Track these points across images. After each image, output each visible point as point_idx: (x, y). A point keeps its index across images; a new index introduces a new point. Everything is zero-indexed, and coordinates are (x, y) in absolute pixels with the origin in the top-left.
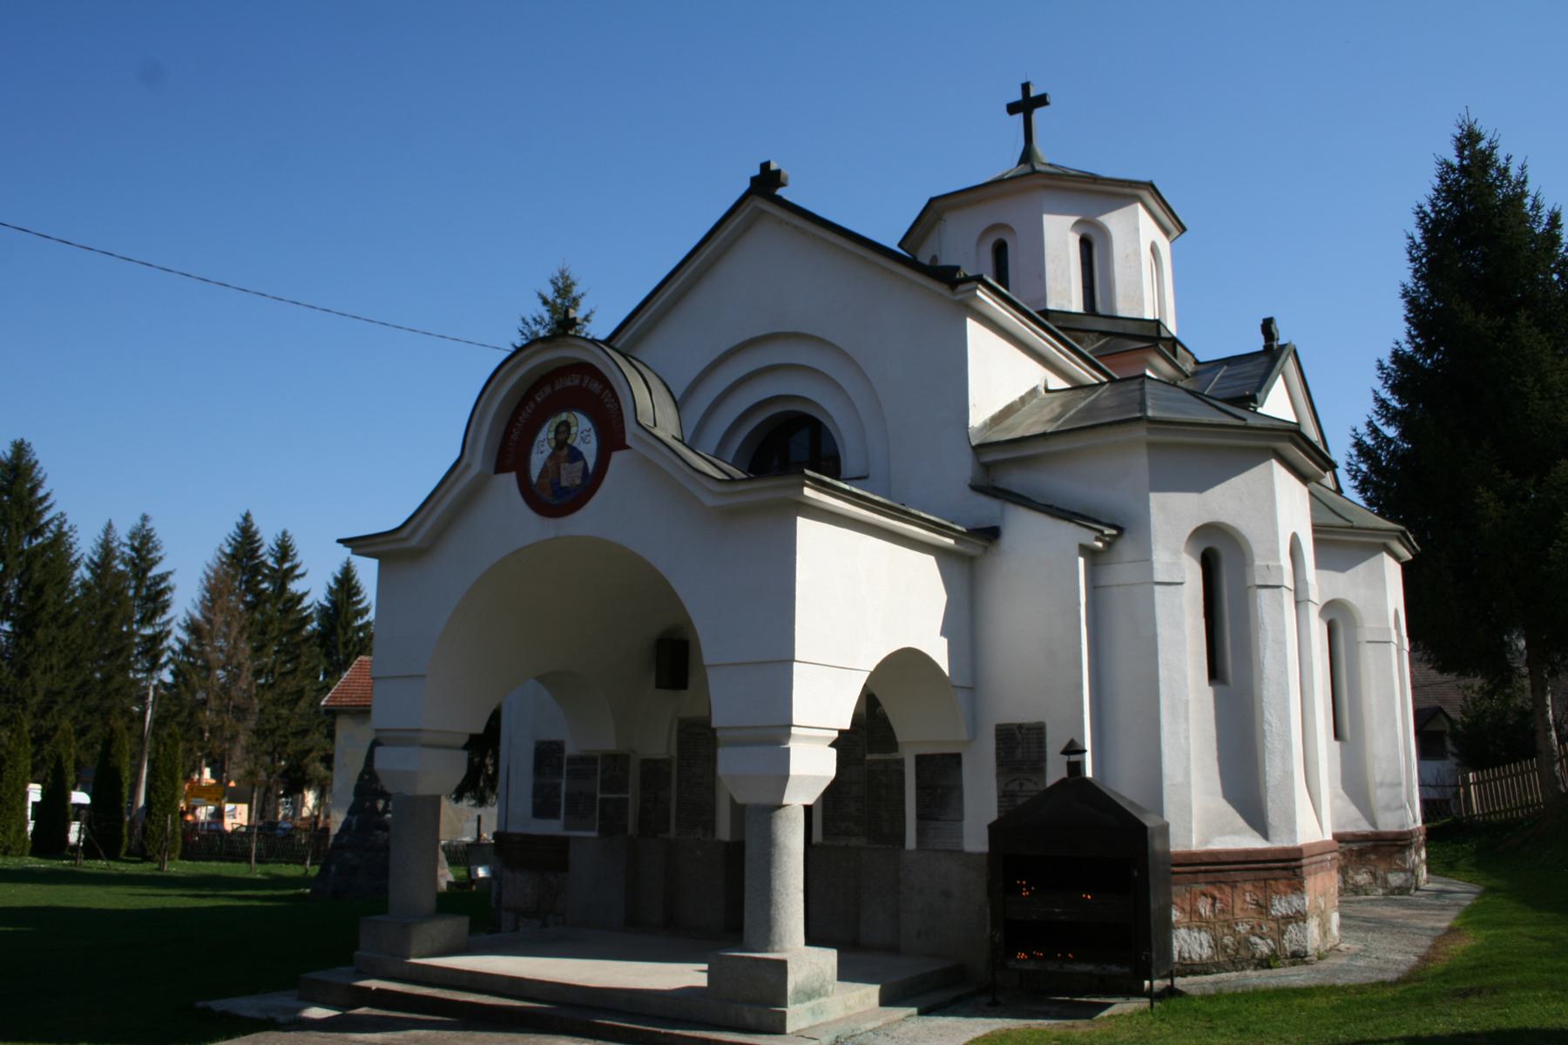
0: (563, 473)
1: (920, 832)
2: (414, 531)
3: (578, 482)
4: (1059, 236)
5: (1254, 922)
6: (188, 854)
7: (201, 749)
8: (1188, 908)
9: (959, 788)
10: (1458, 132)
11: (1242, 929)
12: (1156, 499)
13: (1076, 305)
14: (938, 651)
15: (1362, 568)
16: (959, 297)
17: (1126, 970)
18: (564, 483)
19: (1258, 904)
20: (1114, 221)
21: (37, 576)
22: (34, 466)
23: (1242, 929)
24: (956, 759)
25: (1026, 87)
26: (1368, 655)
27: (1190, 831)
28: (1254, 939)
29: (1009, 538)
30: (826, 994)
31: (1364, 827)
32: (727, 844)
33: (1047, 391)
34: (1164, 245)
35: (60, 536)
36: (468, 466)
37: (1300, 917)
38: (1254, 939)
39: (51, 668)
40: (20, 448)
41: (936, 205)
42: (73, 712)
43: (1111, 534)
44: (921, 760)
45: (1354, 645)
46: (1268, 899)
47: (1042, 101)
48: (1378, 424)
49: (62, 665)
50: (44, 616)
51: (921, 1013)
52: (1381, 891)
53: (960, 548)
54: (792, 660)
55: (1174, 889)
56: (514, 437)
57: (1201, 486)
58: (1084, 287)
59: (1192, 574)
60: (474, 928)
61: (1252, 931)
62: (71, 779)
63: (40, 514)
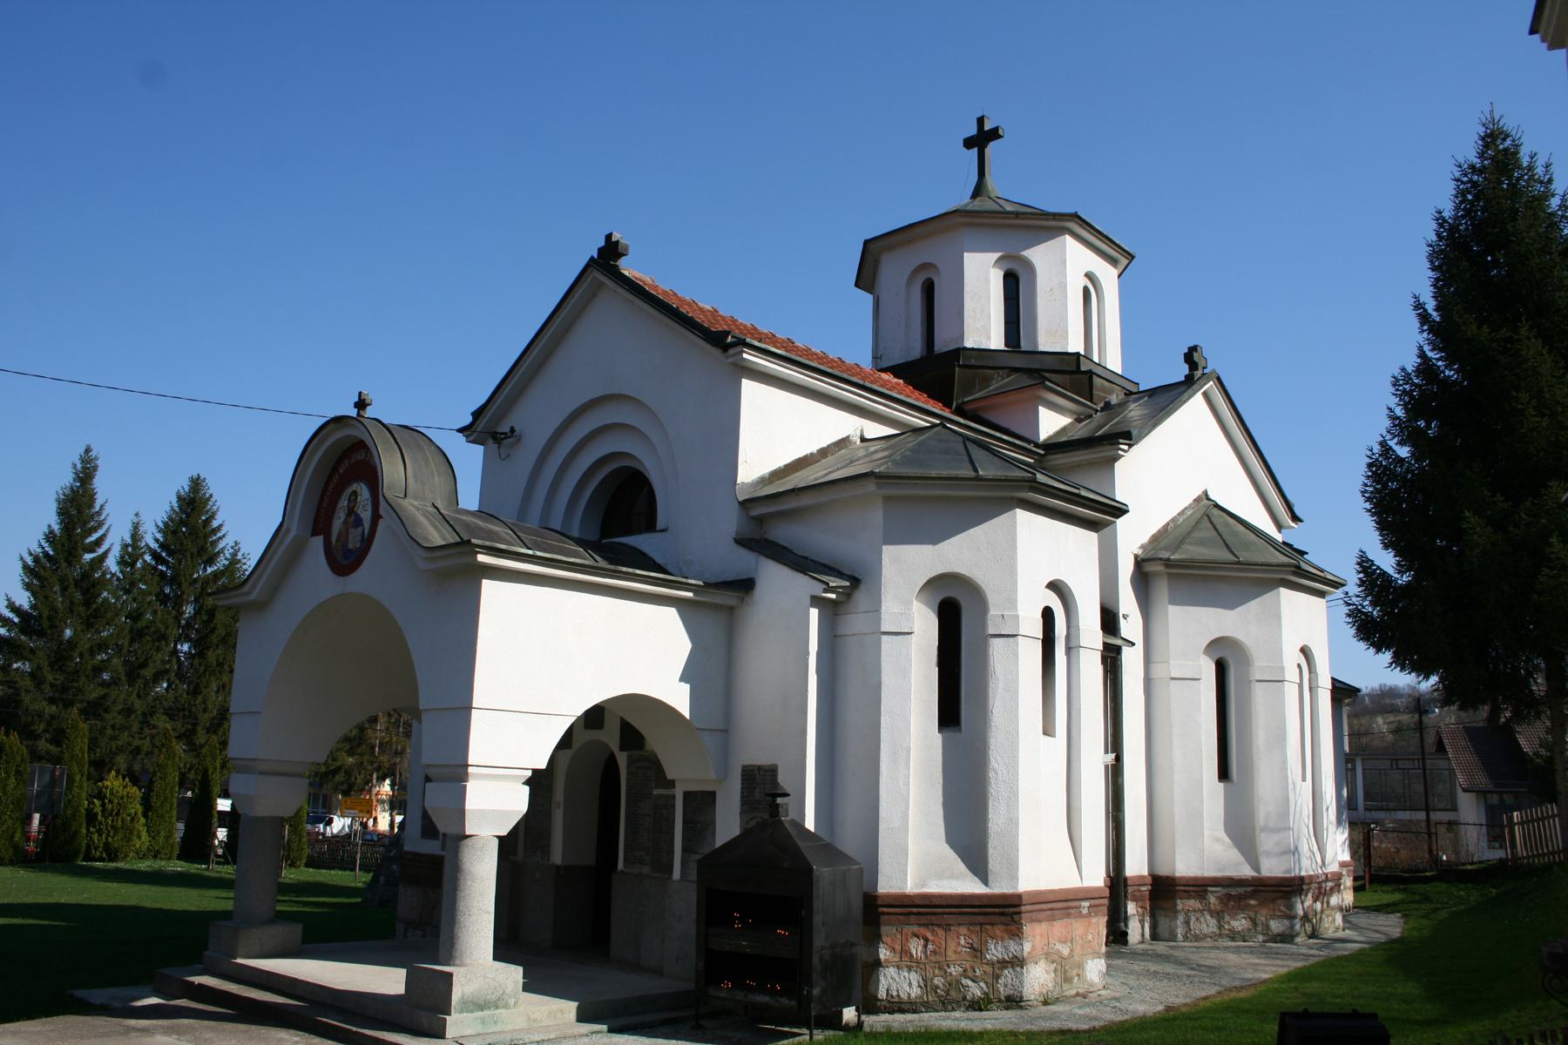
2: (254, 587)
4: (981, 276)
5: (968, 966)
6: (312, 863)
7: (372, 763)
8: (898, 948)
9: (714, 823)
10: (1482, 130)
11: (954, 970)
12: (888, 552)
13: (996, 341)
14: (679, 698)
15: (1254, 606)
17: (793, 1003)
18: (350, 546)
19: (972, 947)
20: (1039, 255)
23: (954, 970)
25: (981, 121)
26: (1260, 694)
27: (906, 874)
28: (964, 981)
30: (506, 1006)
31: (1247, 872)
32: (558, 867)
33: (863, 440)
34: (1108, 275)
35: (234, 561)
36: (288, 531)
37: (1018, 962)
38: (964, 981)
41: (871, 246)
43: (846, 587)
44: (687, 795)
45: (1246, 683)
46: (984, 943)
47: (995, 134)
48: (1392, 443)
50: (214, 639)
51: (611, 1031)
52: (1261, 938)
54: (471, 708)
55: (884, 929)
57: (935, 538)
58: (1006, 323)
59: (925, 626)
61: (965, 974)
62: (217, 790)
63: (214, 543)
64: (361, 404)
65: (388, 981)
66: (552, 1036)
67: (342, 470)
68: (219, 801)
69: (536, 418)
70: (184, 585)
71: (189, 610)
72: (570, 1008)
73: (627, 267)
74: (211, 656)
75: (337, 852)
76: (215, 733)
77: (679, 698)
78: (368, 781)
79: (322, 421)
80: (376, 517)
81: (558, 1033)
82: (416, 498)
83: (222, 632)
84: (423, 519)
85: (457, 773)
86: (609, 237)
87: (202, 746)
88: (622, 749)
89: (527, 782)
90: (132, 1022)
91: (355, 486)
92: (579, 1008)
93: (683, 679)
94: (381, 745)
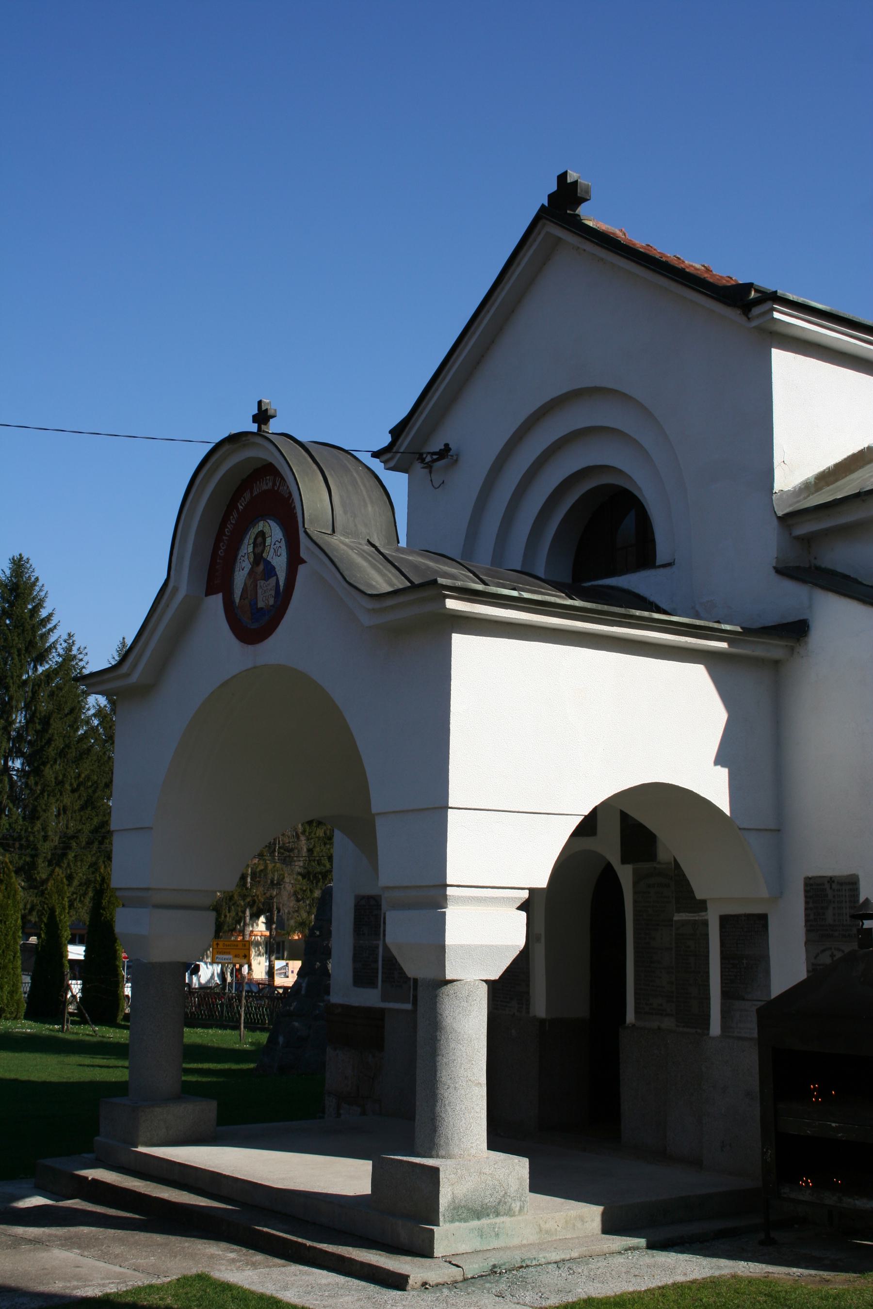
0: (259, 591)
1: (726, 1014)
2: (135, 666)
3: (271, 601)
7: (244, 897)
9: (764, 958)
14: (715, 787)
16: (754, 324)
18: (260, 604)
21: (44, 707)
22: (34, 584)
24: (762, 920)
29: (818, 635)
30: (510, 1213)
32: (542, 1022)
35: (68, 658)
36: (176, 590)
39: (65, 809)
40: (19, 565)
42: (90, 859)
44: (724, 920)
49: (76, 808)
50: (51, 752)
51: (651, 1246)
53: (734, 650)
54: (446, 807)
56: (221, 553)
60: (224, 1118)
62: (67, 934)
63: (45, 637)
64: (262, 416)
65: (347, 1177)
66: (575, 1254)
67: (243, 501)
68: (71, 948)
69: (478, 430)
70: (13, 689)
71: (19, 719)
72: (591, 1215)
73: (591, 215)
74: (48, 772)
75: (213, 1007)
76: (58, 865)
77: (715, 787)
78: (240, 919)
79: (210, 447)
80: (295, 560)
81: (583, 1250)
82: (346, 534)
83: (59, 743)
84: (364, 564)
85: (433, 896)
86: (562, 178)
87: (44, 882)
88: (624, 861)
89: (524, 906)
90: (20, 1230)
91: (260, 526)
92: (604, 1214)
93: (720, 760)
94: (254, 875)
